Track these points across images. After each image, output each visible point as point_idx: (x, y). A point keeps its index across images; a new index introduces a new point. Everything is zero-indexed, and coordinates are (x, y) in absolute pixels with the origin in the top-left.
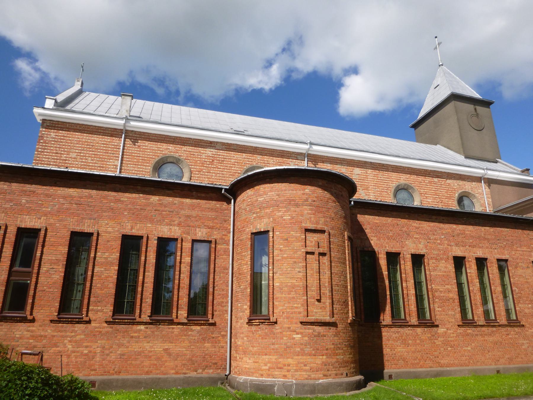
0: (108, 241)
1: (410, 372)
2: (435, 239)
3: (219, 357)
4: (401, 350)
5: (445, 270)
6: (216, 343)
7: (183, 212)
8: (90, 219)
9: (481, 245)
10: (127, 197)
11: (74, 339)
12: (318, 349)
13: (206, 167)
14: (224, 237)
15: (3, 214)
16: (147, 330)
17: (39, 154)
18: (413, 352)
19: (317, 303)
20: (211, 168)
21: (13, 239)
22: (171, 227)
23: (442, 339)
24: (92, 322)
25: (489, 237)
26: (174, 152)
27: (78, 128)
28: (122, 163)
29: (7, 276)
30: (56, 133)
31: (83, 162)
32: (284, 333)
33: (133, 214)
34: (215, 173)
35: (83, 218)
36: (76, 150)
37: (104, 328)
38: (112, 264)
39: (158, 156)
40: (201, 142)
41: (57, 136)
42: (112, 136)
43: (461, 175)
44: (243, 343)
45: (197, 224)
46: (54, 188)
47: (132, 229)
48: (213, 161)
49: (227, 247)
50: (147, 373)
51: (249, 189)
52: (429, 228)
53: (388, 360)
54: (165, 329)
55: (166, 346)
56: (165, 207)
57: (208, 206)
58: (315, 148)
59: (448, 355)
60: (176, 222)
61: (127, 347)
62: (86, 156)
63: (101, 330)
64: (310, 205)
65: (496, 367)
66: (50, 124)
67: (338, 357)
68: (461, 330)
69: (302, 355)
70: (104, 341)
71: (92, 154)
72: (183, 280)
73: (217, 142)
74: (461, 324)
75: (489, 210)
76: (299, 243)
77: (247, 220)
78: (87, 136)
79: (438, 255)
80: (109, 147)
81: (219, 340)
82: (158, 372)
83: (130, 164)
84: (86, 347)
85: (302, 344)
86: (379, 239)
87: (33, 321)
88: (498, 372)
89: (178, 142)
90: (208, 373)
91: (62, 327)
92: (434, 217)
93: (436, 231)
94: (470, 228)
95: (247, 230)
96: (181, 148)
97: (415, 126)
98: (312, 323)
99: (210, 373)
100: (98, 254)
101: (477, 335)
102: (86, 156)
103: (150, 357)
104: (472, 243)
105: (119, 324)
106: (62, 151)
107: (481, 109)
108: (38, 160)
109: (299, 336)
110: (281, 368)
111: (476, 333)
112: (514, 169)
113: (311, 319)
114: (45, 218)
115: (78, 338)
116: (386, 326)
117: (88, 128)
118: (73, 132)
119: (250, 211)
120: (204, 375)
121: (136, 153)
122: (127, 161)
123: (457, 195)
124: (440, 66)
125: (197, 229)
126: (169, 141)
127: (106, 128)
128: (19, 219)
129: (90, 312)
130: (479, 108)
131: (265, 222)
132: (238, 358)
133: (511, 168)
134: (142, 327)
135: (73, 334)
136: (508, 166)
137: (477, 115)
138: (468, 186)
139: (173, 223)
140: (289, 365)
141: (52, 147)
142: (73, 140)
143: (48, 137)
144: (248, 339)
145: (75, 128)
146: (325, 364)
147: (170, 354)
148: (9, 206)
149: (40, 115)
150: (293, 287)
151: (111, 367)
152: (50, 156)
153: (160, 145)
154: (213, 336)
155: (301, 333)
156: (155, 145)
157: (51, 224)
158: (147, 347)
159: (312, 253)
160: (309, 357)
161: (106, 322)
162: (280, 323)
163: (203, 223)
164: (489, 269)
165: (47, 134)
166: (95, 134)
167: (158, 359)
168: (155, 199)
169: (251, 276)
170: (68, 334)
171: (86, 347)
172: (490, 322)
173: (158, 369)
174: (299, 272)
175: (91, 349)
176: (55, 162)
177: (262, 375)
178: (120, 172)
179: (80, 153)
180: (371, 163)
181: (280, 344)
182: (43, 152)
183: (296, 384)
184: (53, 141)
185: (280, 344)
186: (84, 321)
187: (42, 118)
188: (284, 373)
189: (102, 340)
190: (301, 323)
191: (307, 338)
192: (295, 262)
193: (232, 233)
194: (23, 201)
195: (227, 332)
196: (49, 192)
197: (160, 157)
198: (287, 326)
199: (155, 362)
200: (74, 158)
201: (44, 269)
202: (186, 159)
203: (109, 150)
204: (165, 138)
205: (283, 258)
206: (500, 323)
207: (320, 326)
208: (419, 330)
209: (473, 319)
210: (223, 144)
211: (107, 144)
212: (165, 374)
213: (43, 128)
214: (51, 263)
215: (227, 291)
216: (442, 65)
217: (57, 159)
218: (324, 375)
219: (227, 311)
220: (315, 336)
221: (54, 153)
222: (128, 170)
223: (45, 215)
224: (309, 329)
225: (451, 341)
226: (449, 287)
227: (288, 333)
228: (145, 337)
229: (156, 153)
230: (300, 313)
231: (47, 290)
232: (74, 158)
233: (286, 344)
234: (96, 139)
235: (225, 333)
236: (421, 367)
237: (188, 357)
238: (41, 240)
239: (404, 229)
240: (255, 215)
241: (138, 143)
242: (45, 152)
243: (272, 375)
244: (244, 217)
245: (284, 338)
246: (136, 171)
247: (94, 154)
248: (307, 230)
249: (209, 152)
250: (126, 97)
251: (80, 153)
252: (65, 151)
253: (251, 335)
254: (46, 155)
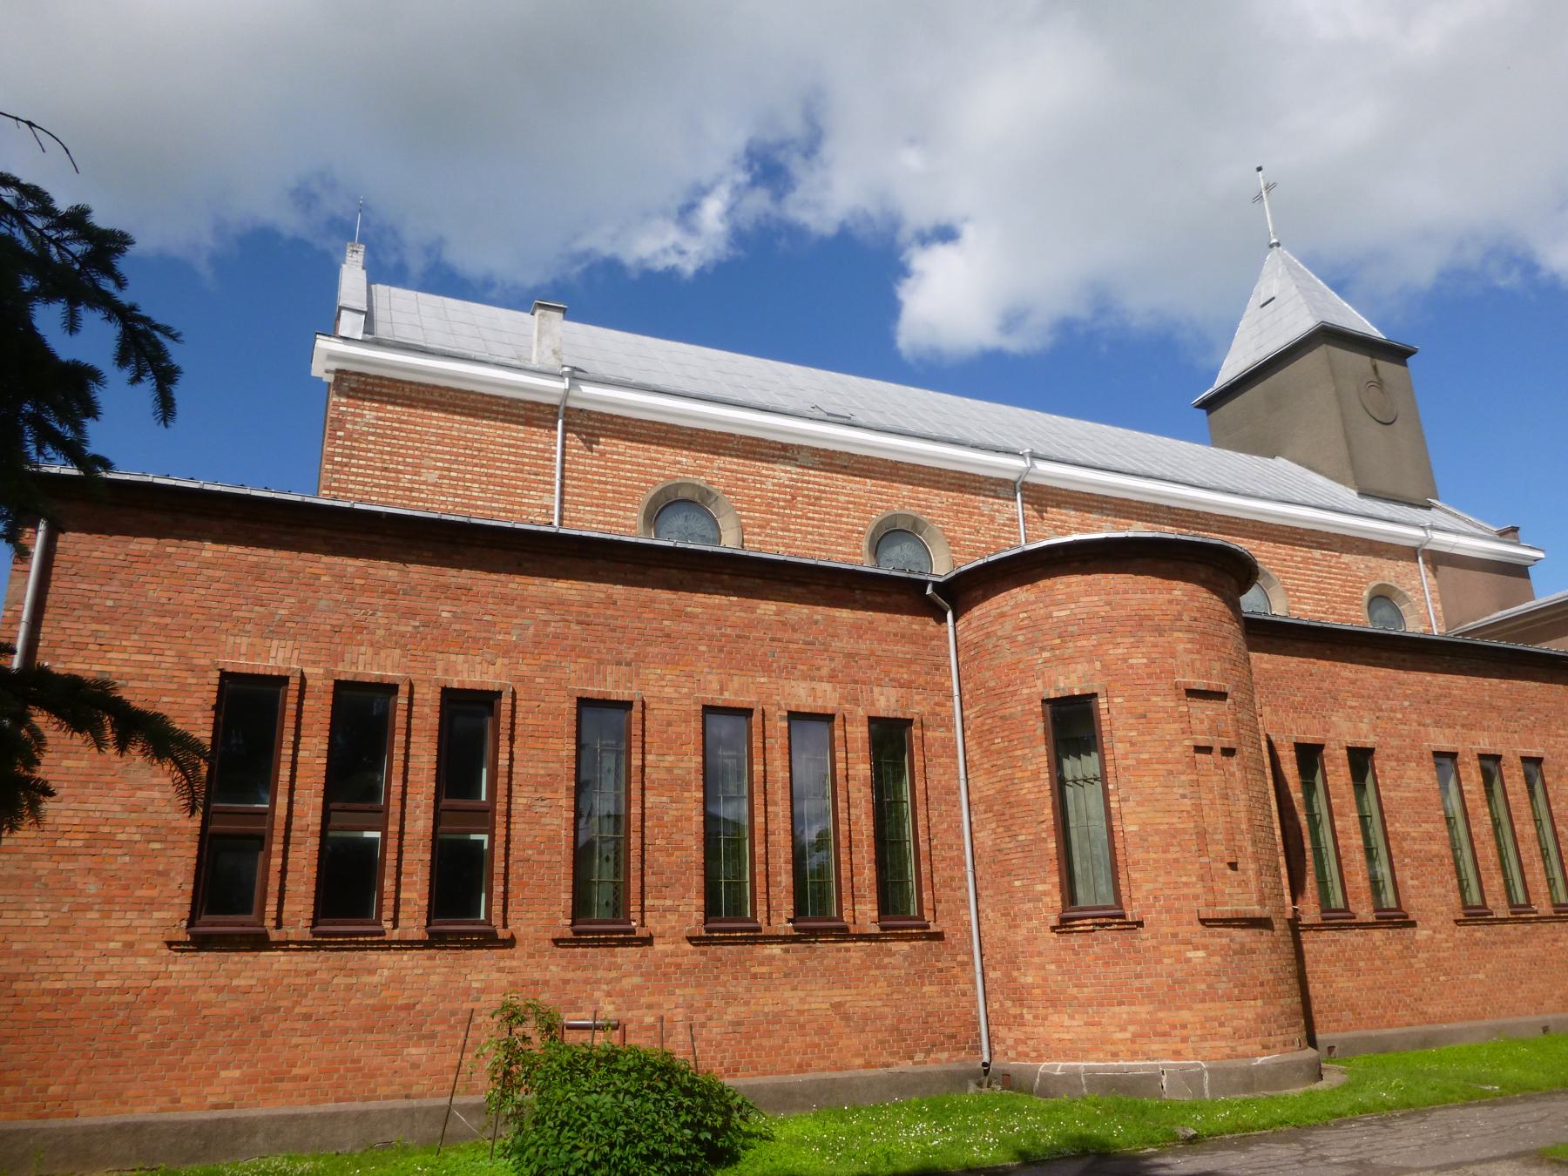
0: (669, 724)
1: (1370, 1038)
2: (1392, 710)
3: (958, 1019)
4: (1344, 983)
5: (1418, 785)
7: (836, 644)
8: (619, 663)
9: (1485, 723)
10: (704, 606)
11: (618, 987)
12: (1244, 985)
13: (777, 514)
15: (398, 651)
16: (788, 956)
17: (338, 472)
18: (1370, 989)
19: (1229, 872)
20: (789, 516)
21: (434, 720)
22: (814, 684)
23: (1426, 955)
24: (656, 940)
25: (1500, 703)
26: (694, 473)
27: (436, 397)
28: (562, 501)
29: (431, 823)
30: (377, 410)
32: (1164, 948)
33: (721, 650)
34: (800, 532)
35: (601, 662)
36: (436, 460)
37: (685, 954)
38: (686, 786)
39: (654, 483)
40: (759, 446)
42: (528, 422)
43: (1371, 542)
44: (1045, 979)
45: (873, 674)
46: (518, 579)
47: (722, 691)
48: (794, 498)
49: (949, 735)
50: (801, 1068)
51: (1020, 584)
52: (1376, 683)
53: (1320, 1012)
54: (828, 952)
55: (838, 995)
56: (794, 630)
57: (892, 627)
58: (1042, 466)
59: (1441, 994)
60: (825, 672)
61: (747, 1003)
62: (465, 480)
63: (679, 960)
64: (1189, 630)
65: (1538, 1018)
66: (359, 385)
67: (1282, 1001)
68: (1462, 932)
69: (1212, 1000)
70: (689, 991)
71: (480, 474)
72: (856, 823)
73: (800, 447)
74: (1462, 917)
75: (1437, 630)
76: (1176, 726)
77: (1021, 666)
78: (462, 423)
79: (1401, 749)
80: (525, 456)
81: (955, 977)
82: (822, 1064)
83: (583, 504)
84: (650, 1007)
85: (1208, 974)
86: (1275, 711)
87: (510, 943)
88: (1545, 1030)
89: (702, 445)
90: (937, 1061)
91: (584, 955)
92: (1385, 655)
93: (1391, 688)
94: (1461, 680)
95: (1025, 691)
96: (712, 461)
97: (1210, 405)
98: (1227, 922)
99: (942, 1061)
100: (649, 758)
101: (1494, 943)
102: (465, 480)
103: (802, 1027)
104: (1466, 718)
105: (721, 942)
106: (398, 463)
107: (1386, 368)
108: (335, 489)
109: (1201, 954)
110: (1164, 1034)
111: (1492, 938)
112: (1480, 527)
113: (1225, 910)
114: (506, 661)
115: (627, 983)
116: (1310, 927)
117: (464, 399)
118: (424, 408)
119: (1030, 643)
120: (931, 1067)
121: (596, 474)
122: (574, 495)
123: (1366, 593)
124: (1271, 246)
126: (677, 441)
127: (512, 400)
128: (440, 665)
129: (647, 914)
130: (1383, 365)
131: (1080, 673)
132: (1029, 1017)
133: (1469, 522)
134: (776, 950)
135: (613, 974)
136: (1463, 519)
137: (1380, 384)
138: (1389, 571)
139: (816, 673)
140: (1184, 1027)
141: (370, 451)
142: (426, 433)
143: (355, 423)
144: (1059, 967)
145: (429, 397)
146: (1260, 1018)
147: (846, 1018)
148: (410, 629)
149: (332, 357)
150: (1174, 833)
151: (713, 1058)
152: (368, 476)
153: (657, 452)
154: (940, 965)
155: (1205, 947)
156: (644, 450)
157: (521, 679)
158: (794, 1002)
159: (1207, 750)
160: (1227, 1004)
161: (690, 939)
162: (1152, 924)
163: (887, 673)
164: (1507, 781)
165: (353, 414)
166: (483, 418)
167: (822, 1031)
168: (767, 609)
169: (1054, 808)
170: (601, 974)
171: (650, 1007)
172: (1521, 913)
173: (823, 1058)
174: (1184, 796)
175: (662, 1012)
176: (381, 495)
177: (1115, 1055)
178: (561, 524)
179: (449, 470)
180: (1169, 507)
181: (1158, 975)
182: (346, 465)
183: (1210, 1071)
184: (373, 434)
185: (1158, 975)
186: (638, 939)
187: (334, 366)
188: (1174, 1047)
189: (685, 985)
190: (1203, 921)
191: (1217, 959)
192: (1170, 773)
193: (957, 699)
194: (444, 614)
195: (972, 953)
196: (507, 591)
197: (660, 487)
198: (1170, 930)
199: (817, 1040)
201: (520, 801)
203: (524, 464)
204: (667, 432)
205: (1139, 761)
206: (1540, 914)
207: (1243, 927)
208: (1377, 935)
209: (1484, 906)
210: (815, 452)
211: (518, 447)
212: (840, 1069)
213: (339, 394)
214: (539, 785)
215: (961, 849)
216: (1278, 245)
217: (388, 487)
218: (1265, 1047)
219: (965, 901)
220: (1235, 953)
221: (375, 469)
222: (580, 520)
223: (506, 654)
224: (1220, 935)
225: (1445, 959)
226: (1429, 827)
227: (1172, 948)
228: (786, 975)
229: (647, 473)
230: (1196, 897)
231: (536, 857)
232: (434, 485)
233: (1170, 975)
234: (488, 430)
235: (966, 958)
236: (1390, 1026)
237: (888, 1022)
238: (505, 722)
239: (1326, 685)
240: (1046, 654)
241: (598, 443)
242: (354, 466)
243: (1144, 1054)
244: (1008, 657)
245: (1166, 961)
246: (599, 522)
247: (486, 475)
248: (1192, 693)
249: (783, 473)
250: (550, 313)
252: (408, 464)
253: (1069, 956)
254: (357, 475)
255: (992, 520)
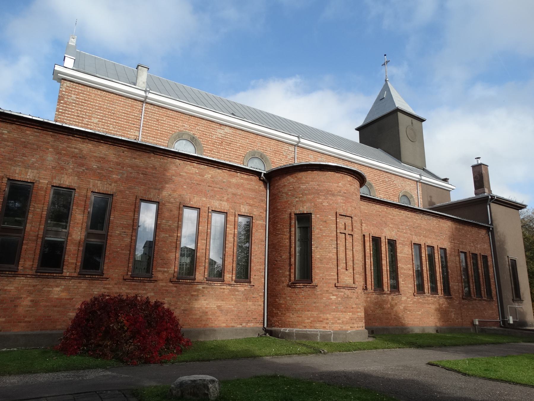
6: (256, 301)
7: (230, 190)
8: (155, 189)
12: (347, 308)
14: (261, 214)
17: (60, 115)
20: (220, 148)
22: (221, 202)
31: (105, 128)
33: (191, 188)
35: (149, 188)
36: (98, 115)
37: (170, 286)
41: (77, 98)
45: (241, 201)
55: (219, 303)
60: (225, 198)
63: (167, 289)
86: (367, 226)
96: (196, 127)
106: (83, 115)
109: (335, 297)
110: (321, 321)
114: (116, 184)
121: (155, 126)
125: (242, 206)
128: (91, 184)
139: (223, 199)
142: (95, 105)
143: (68, 99)
147: (221, 310)
152: (72, 118)
154: (254, 296)
155: (336, 295)
158: (205, 304)
165: (67, 95)
177: (305, 327)
179: (102, 119)
182: (64, 113)
184: (74, 103)
200: (96, 124)
202: (199, 138)
203: (129, 120)
211: (128, 114)
217: (79, 123)
227: (327, 295)
231: (121, 252)
232: (96, 124)
240: (297, 199)
242: (66, 114)
251: (102, 119)
252: (87, 115)
254: (68, 117)
255: (286, 157)
